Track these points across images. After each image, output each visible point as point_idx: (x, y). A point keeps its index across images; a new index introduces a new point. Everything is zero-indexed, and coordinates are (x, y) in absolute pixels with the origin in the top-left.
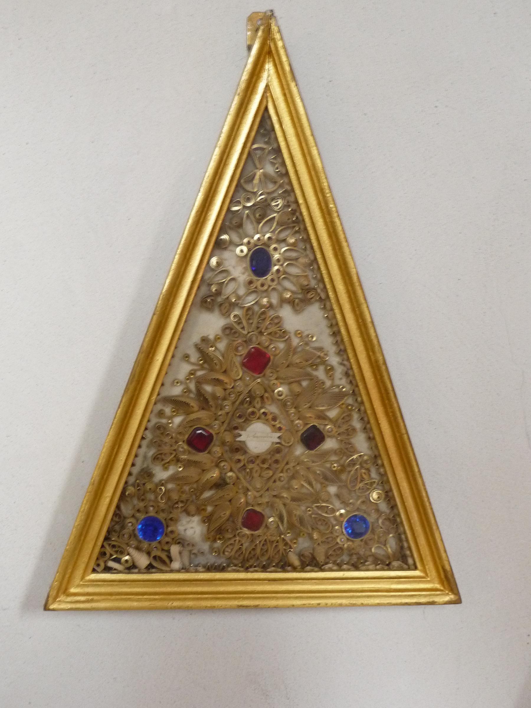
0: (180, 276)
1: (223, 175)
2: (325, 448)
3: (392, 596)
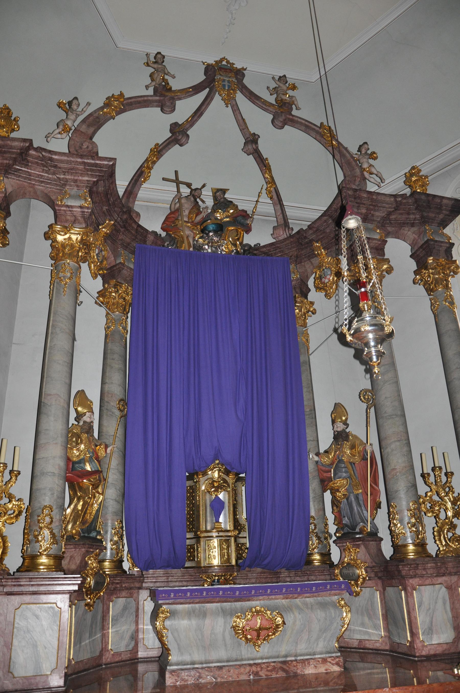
3: (294, 473)
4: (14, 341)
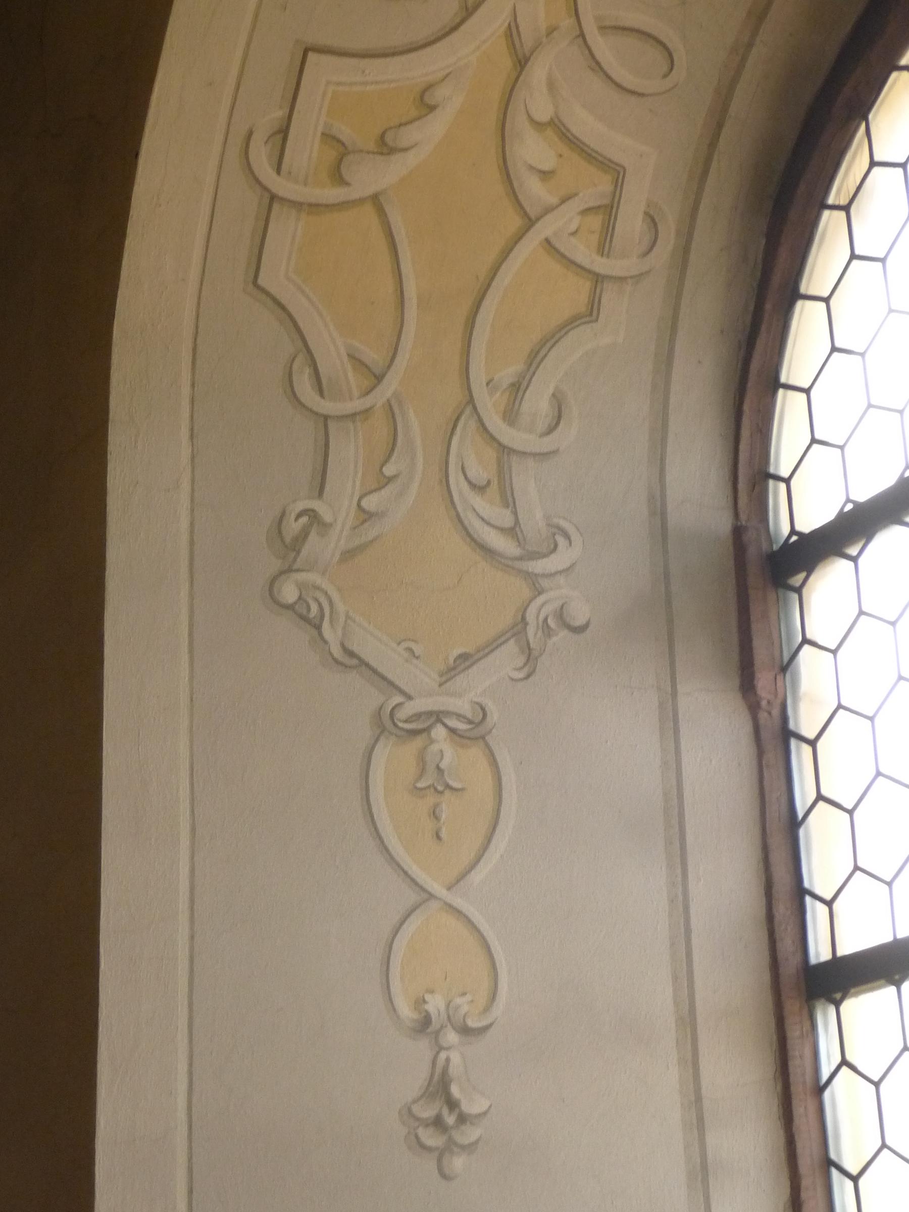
1: (773, 1003)
4: (888, 938)
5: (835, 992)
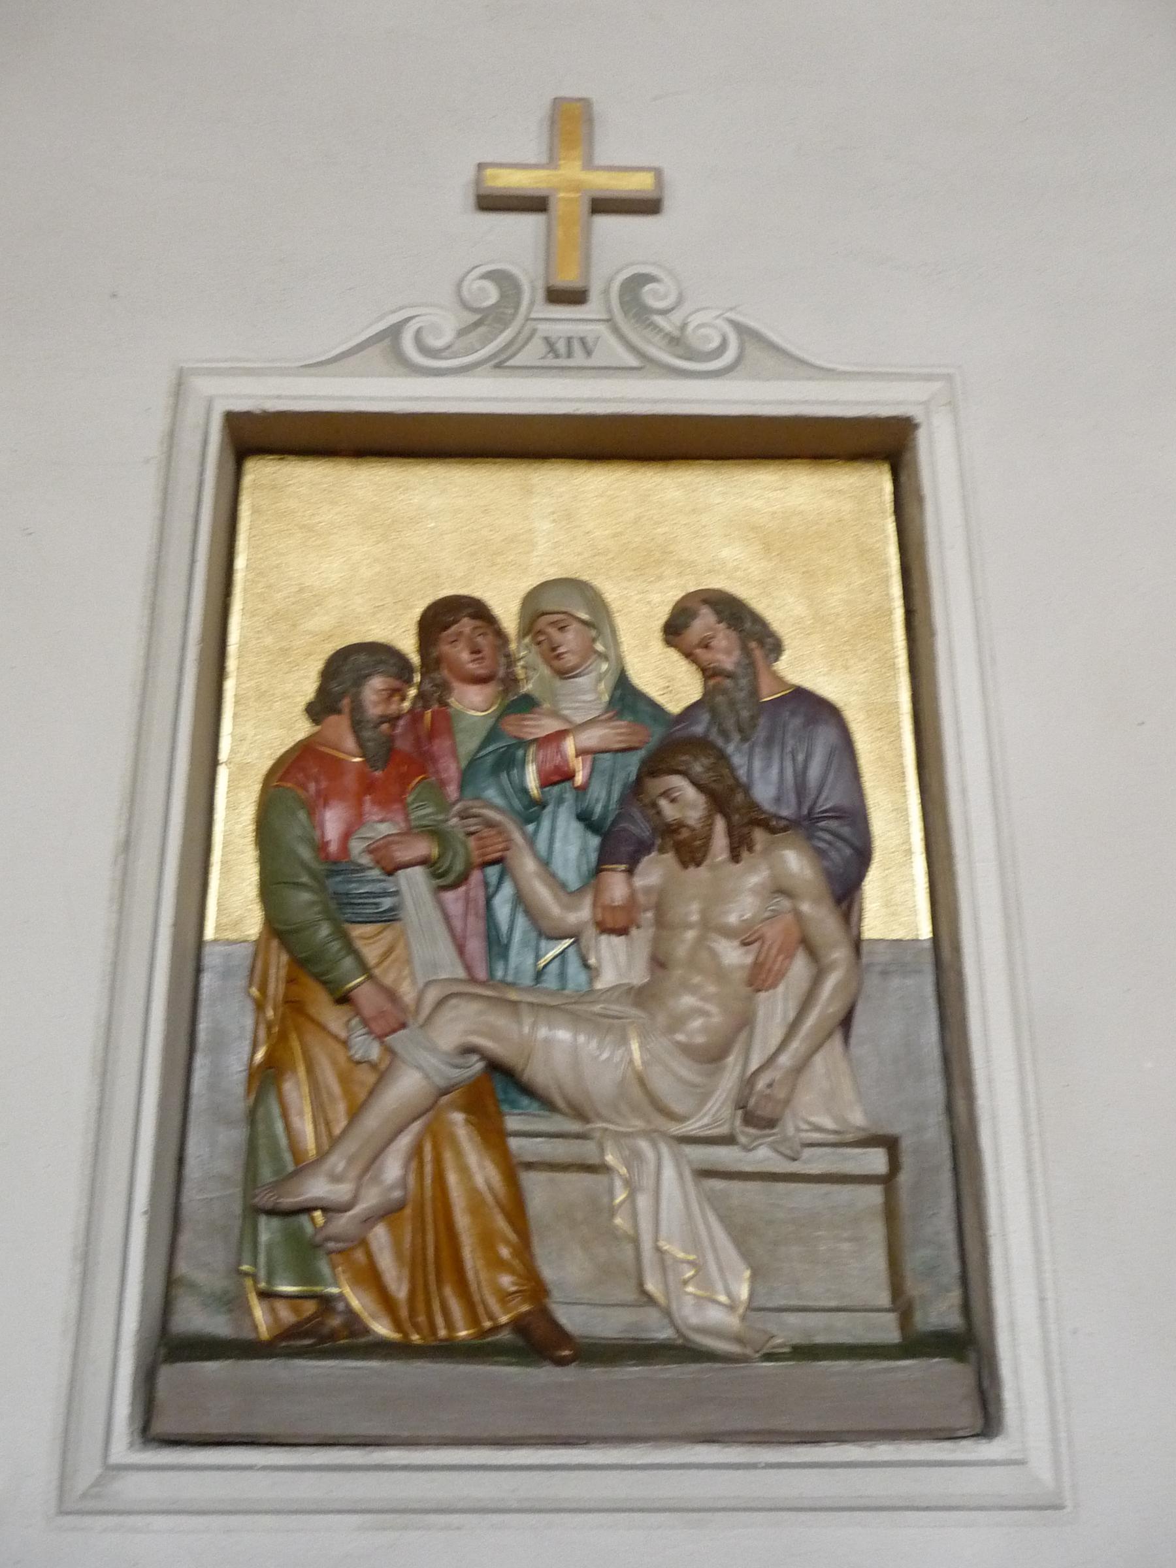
0: (708, 1127)
1: (823, 983)
2: (347, 989)
5: (612, 1155)
